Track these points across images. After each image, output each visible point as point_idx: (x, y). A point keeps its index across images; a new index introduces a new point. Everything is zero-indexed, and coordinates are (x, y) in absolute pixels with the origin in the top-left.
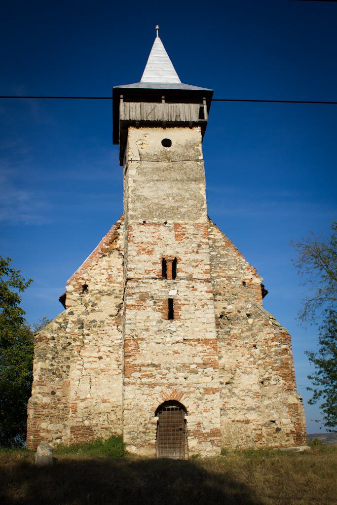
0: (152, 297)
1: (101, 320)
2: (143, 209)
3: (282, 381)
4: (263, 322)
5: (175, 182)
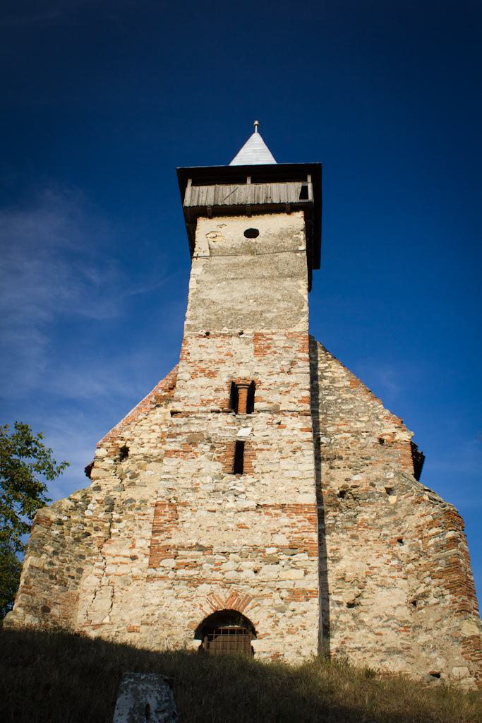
0: (209, 439)
1: (143, 499)
2: (208, 316)
3: (449, 597)
4: (413, 498)
5: (259, 280)
